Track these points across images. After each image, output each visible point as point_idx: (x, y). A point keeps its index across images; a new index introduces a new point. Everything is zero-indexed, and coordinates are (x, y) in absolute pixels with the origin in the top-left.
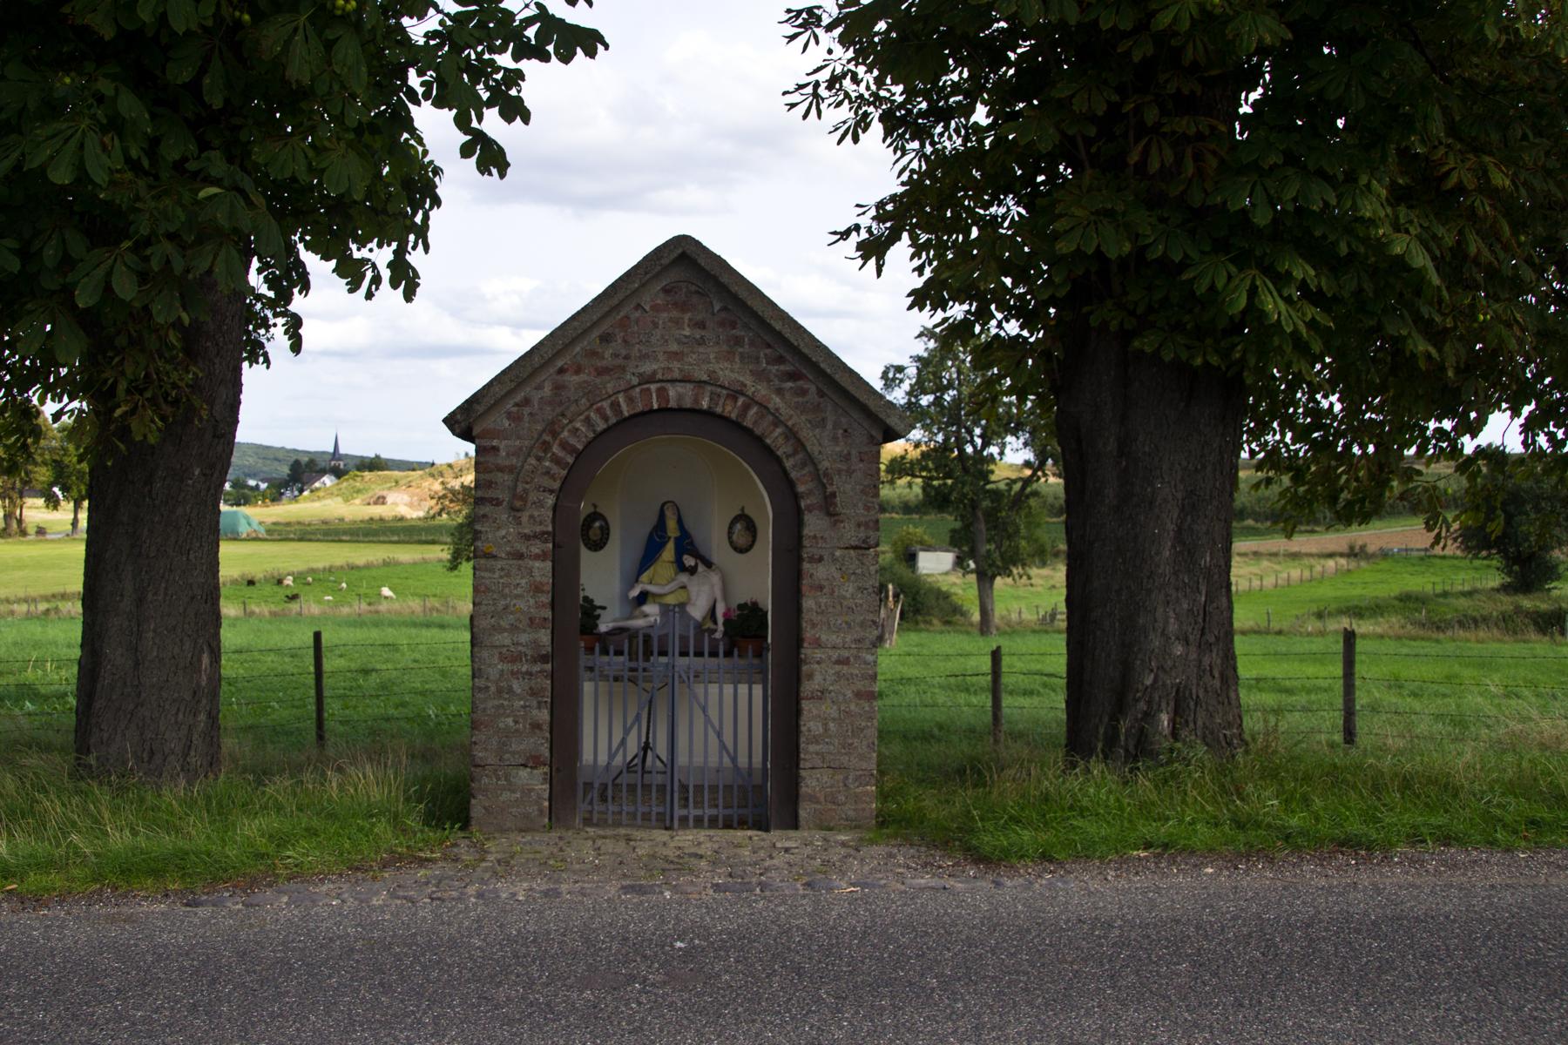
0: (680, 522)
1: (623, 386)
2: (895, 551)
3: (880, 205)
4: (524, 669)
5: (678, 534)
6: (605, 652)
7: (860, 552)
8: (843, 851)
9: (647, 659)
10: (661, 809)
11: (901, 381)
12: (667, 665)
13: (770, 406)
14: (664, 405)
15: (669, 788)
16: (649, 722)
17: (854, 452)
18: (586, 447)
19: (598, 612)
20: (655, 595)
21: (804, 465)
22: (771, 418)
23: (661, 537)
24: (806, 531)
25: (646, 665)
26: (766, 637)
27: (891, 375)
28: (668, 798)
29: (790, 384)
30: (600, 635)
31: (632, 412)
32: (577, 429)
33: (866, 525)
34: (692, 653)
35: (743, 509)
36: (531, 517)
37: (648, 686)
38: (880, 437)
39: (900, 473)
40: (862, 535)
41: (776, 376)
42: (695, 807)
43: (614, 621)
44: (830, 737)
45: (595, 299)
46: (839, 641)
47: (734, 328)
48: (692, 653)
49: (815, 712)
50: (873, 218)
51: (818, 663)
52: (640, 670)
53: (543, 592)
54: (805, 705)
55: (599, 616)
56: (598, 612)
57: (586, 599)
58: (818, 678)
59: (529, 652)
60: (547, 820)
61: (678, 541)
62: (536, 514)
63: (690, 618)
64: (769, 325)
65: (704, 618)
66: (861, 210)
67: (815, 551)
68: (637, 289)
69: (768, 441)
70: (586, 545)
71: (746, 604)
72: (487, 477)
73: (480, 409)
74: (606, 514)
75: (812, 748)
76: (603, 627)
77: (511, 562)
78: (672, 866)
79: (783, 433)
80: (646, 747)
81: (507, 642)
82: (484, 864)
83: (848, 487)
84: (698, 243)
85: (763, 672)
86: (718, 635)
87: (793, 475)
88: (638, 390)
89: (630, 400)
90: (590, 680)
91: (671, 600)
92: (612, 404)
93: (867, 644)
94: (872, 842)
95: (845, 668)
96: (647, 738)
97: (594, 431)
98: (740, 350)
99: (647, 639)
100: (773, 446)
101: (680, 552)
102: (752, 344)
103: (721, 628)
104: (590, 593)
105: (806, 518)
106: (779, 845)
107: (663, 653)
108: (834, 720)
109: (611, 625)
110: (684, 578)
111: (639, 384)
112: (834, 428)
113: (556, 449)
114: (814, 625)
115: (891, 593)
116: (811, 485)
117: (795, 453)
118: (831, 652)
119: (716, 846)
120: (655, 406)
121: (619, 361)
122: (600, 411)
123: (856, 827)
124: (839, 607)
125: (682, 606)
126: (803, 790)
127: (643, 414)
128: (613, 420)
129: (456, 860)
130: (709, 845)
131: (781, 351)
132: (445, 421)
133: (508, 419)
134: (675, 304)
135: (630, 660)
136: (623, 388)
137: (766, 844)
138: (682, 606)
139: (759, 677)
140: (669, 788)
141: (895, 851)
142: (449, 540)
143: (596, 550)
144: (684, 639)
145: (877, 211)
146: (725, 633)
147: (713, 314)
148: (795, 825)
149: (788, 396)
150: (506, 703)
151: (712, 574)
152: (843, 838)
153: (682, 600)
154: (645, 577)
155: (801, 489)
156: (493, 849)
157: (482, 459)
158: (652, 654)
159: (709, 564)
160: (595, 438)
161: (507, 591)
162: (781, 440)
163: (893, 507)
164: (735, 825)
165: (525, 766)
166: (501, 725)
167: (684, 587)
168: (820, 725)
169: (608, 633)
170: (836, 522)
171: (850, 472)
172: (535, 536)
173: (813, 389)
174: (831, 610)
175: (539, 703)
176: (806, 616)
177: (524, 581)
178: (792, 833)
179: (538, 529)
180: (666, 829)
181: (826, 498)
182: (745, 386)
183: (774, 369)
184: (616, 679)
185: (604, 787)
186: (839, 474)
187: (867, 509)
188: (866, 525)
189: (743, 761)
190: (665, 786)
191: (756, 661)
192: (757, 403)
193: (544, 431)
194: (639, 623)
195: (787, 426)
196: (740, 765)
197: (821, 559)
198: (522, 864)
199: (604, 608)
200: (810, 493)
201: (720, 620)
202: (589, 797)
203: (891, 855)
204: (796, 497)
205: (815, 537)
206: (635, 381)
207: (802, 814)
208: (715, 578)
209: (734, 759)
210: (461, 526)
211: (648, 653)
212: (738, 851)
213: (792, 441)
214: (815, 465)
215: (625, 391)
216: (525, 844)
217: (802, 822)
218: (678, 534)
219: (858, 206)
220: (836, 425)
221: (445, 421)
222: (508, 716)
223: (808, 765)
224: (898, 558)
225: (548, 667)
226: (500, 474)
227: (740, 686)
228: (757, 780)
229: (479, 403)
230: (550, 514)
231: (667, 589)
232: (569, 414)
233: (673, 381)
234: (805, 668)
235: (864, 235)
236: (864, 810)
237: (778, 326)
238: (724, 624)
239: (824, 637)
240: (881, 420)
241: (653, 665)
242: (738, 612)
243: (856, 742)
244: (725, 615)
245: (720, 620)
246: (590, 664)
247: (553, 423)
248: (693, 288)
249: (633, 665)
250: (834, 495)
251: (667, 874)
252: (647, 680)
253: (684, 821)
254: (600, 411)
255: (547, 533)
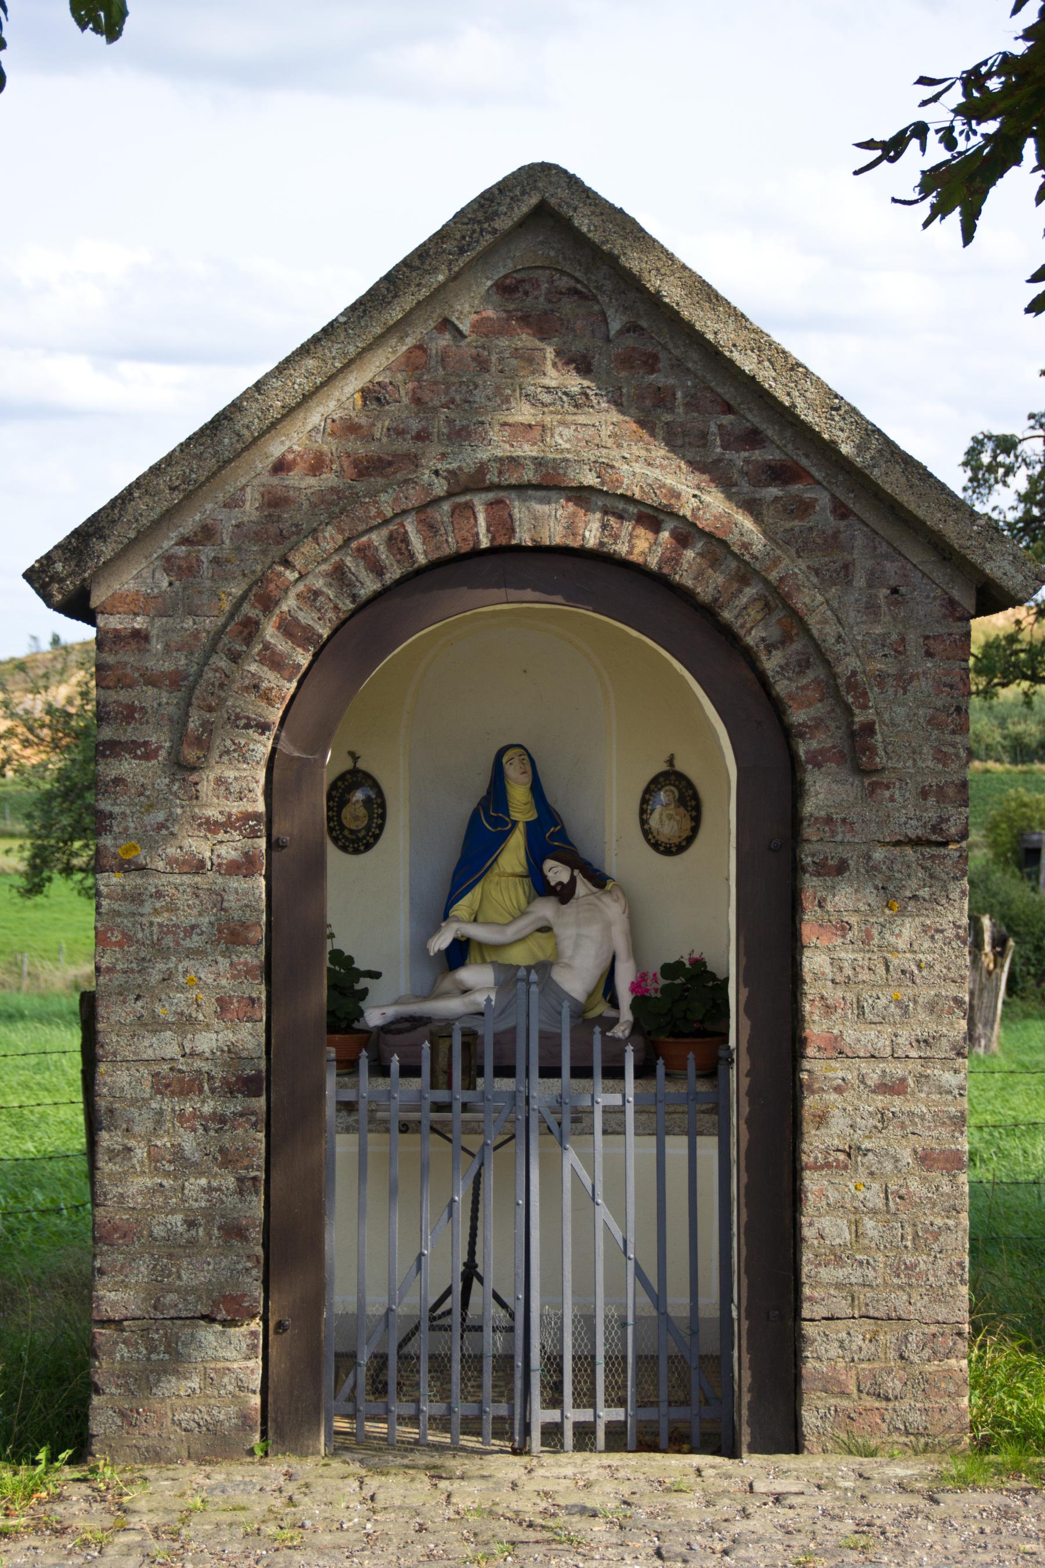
0: (537, 789)
1: (414, 497)
2: (994, 845)
3: (973, 79)
4: (207, 1109)
5: (532, 816)
6: (380, 1069)
7: (928, 851)
8: (904, 1501)
9: (469, 1085)
10: (503, 1410)
11: (1010, 470)
12: (514, 1096)
13: (732, 539)
14: (502, 541)
15: (519, 1363)
16: (474, 1218)
17: (913, 637)
18: (335, 632)
19: (364, 983)
20: (481, 946)
21: (804, 665)
22: (734, 565)
23: (496, 822)
24: (810, 807)
25: (468, 1096)
26: (726, 1035)
27: (986, 458)
28: (519, 1384)
29: (774, 491)
30: (367, 1032)
31: (435, 556)
32: (317, 594)
33: (941, 793)
34: (566, 1071)
35: (671, 761)
36: (220, 781)
37: (473, 1142)
38: (967, 601)
39: (1005, 674)
40: (931, 815)
41: (744, 473)
42: (576, 1405)
43: (396, 1003)
44: (866, 1249)
45: (353, 308)
46: (883, 1044)
47: (653, 371)
48: (566, 1071)
49: (833, 1195)
50: (958, 111)
51: (838, 1090)
52: (457, 1107)
53: (246, 942)
54: (813, 1183)
55: (365, 992)
56: (364, 983)
57: (337, 956)
58: (838, 1123)
59: (218, 1073)
60: (257, 1437)
61: (533, 830)
62: (230, 774)
63: (561, 994)
64: (731, 362)
65: (590, 995)
66: (931, 91)
67: (828, 848)
68: (443, 286)
69: (727, 615)
70: (335, 840)
71: (679, 964)
72: (123, 696)
73: (107, 550)
74: (376, 773)
75: (826, 1274)
76: (374, 1017)
77: (177, 879)
78: (532, 1535)
79: (760, 597)
80: (470, 1273)
81: (172, 1050)
82: (123, 1539)
83: (900, 711)
84: (573, 182)
85: (720, 1108)
86: (621, 1031)
87: (782, 687)
88: (446, 507)
89: (430, 528)
90: (348, 1130)
91: (519, 956)
92: (391, 539)
93: (944, 1049)
94: (963, 1482)
95: (897, 1101)
96: (472, 1252)
97: (354, 597)
98: (668, 417)
99: (471, 1040)
100: (736, 626)
101: (536, 854)
102: (691, 404)
103: (626, 1015)
104: (344, 941)
105: (809, 779)
106: (760, 1487)
107: (505, 1071)
108: (874, 1212)
109: (391, 1012)
110: (546, 909)
111: (450, 495)
112: (870, 586)
113: (270, 632)
114: (829, 1009)
115: (987, 937)
116: (819, 709)
117: (785, 640)
118: (864, 1067)
119: (625, 1489)
120: (485, 543)
121: (405, 445)
122: (365, 554)
123: (926, 1447)
124: (881, 970)
125: (544, 968)
126: (810, 1366)
127: (458, 558)
128: (394, 573)
129: (60, 1532)
130: (609, 1487)
131: (755, 419)
132: (30, 576)
133: (167, 571)
134: (525, 320)
135: (434, 1086)
136: (414, 502)
137: (733, 1486)
138: (544, 968)
139: (709, 1120)
140: (519, 1363)
141: (1016, 1503)
142: (21, 827)
143: (357, 851)
144: (550, 1041)
145: (967, 93)
146: (636, 1027)
147: (608, 340)
148: (794, 1444)
149: (769, 515)
150: (167, 1183)
151: (606, 899)
152: (901, 1472)
153: (541, 957)
154: (463, 908)
155: (798, 716)
156: (142, 1505)
157: (110, 659)
158: (481, 1073)
159: (599, 880)
160: (354, 613)
161: (169, 941)
162: (754, 613)
163: (988, 747)
164: (663, 1441)
165: (210, 1319)
166: (158, 1231)
167: (546, 929)
168: (843, 1224)
169: (385, 1029)
170: (874, 787)
171: (904, 680)
172: (228, 824)
173: (824, 499)
174: (865, 975)
175: (240, 1180)
176: (811, 990)
177: (205, 920)
178: (786, 1460)
179: (235, 808)
180: (515, 1452)
181: (852, 735)
182: (678, 496)
183: (739, 458)
184: (405, 1128)
185: (380, 1361)
186: (881, 685)
187: (941, 757)
188: (941, 793)
189: (678, 1302)
190: (511, 1358)
191: (703, 1087)
192: (702, 532)
193: (244, 597)
194: (452, 1006)
195: (766, 582)
196: (672, 1312)
197: (841, 868)
198: (208, 1537)
199: (375, 975)
200: (818, 724)
201: (625, 997)
202: (350, 1381)
203: (1006, 1513)
204: (787, 734)
205: (829, 820)
206: (440, 487)
207: (809, 1418)
208: (613, 909)
209: (659, 1299)
210: (49, 797)
211: (473, 1072)
212: (674, 1499)
213: (779, 614)
214: (827, 664)
215: (421, 509)
216: (211, 1490)
217: (811, 1439)
218: (532, 816)
219: (923, 81)
220: (874, 579)
221: (30, 576)
222: (173, 1211)
223: (821, 1311)
224: (1000, 858)
225: (260, 1103)
226: (150, 691)
227: (669, 1140)
228: (710, 1344)
229: (103, 538)
230: (261, 775)
231: (510, 933)
232: (298, 560)
233: (521, 488)
234: (810, 1103)
235: (937, 153)
236: (942, 1410)
237: (747, 363)
238: (633, 1007)
239: (850, 1036)
240: (973, 566)
241: (483, 1096)
242: (662, 982)
243: (923, 1260)
244: (635, 987)
245: (625, 997)
246: (349, 1096)
247: (262, 580)
248: (564, 283)
249: (441, 1095)
250: (869, 729)
251: (521, 1551)
252: (470, 1129)
253: (552, 1434)
254: (365, 554)
255: (255, 816)
